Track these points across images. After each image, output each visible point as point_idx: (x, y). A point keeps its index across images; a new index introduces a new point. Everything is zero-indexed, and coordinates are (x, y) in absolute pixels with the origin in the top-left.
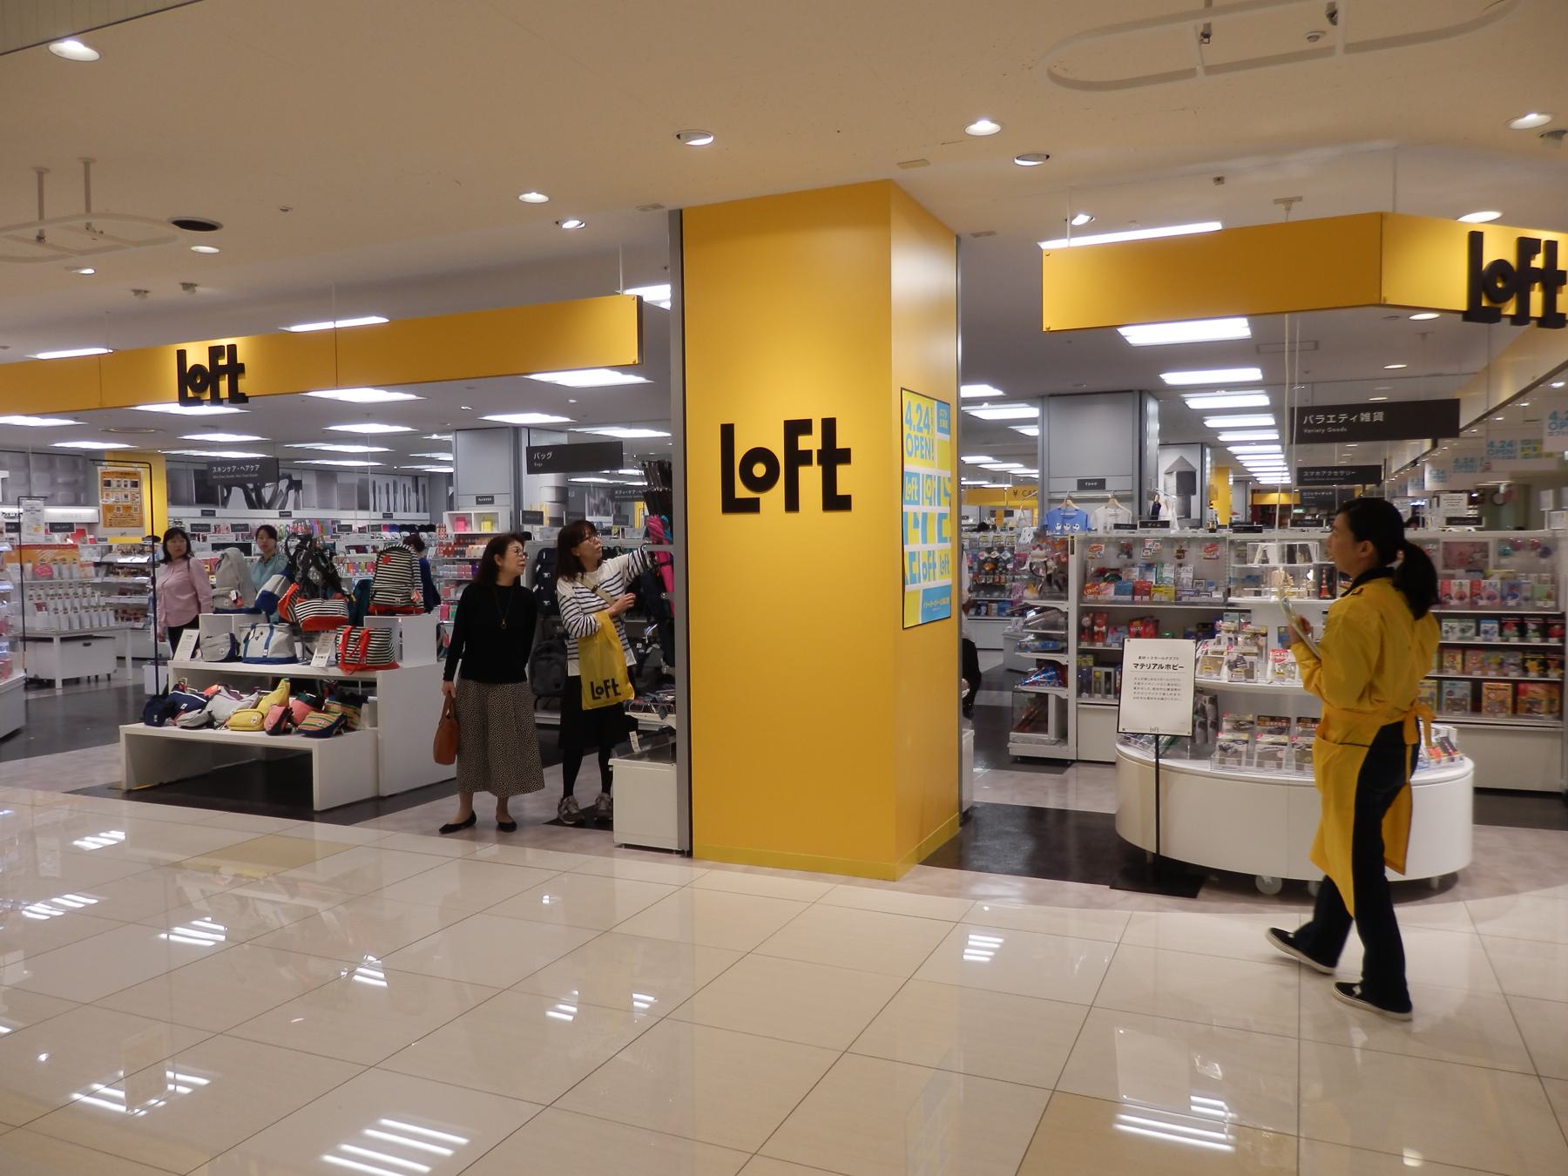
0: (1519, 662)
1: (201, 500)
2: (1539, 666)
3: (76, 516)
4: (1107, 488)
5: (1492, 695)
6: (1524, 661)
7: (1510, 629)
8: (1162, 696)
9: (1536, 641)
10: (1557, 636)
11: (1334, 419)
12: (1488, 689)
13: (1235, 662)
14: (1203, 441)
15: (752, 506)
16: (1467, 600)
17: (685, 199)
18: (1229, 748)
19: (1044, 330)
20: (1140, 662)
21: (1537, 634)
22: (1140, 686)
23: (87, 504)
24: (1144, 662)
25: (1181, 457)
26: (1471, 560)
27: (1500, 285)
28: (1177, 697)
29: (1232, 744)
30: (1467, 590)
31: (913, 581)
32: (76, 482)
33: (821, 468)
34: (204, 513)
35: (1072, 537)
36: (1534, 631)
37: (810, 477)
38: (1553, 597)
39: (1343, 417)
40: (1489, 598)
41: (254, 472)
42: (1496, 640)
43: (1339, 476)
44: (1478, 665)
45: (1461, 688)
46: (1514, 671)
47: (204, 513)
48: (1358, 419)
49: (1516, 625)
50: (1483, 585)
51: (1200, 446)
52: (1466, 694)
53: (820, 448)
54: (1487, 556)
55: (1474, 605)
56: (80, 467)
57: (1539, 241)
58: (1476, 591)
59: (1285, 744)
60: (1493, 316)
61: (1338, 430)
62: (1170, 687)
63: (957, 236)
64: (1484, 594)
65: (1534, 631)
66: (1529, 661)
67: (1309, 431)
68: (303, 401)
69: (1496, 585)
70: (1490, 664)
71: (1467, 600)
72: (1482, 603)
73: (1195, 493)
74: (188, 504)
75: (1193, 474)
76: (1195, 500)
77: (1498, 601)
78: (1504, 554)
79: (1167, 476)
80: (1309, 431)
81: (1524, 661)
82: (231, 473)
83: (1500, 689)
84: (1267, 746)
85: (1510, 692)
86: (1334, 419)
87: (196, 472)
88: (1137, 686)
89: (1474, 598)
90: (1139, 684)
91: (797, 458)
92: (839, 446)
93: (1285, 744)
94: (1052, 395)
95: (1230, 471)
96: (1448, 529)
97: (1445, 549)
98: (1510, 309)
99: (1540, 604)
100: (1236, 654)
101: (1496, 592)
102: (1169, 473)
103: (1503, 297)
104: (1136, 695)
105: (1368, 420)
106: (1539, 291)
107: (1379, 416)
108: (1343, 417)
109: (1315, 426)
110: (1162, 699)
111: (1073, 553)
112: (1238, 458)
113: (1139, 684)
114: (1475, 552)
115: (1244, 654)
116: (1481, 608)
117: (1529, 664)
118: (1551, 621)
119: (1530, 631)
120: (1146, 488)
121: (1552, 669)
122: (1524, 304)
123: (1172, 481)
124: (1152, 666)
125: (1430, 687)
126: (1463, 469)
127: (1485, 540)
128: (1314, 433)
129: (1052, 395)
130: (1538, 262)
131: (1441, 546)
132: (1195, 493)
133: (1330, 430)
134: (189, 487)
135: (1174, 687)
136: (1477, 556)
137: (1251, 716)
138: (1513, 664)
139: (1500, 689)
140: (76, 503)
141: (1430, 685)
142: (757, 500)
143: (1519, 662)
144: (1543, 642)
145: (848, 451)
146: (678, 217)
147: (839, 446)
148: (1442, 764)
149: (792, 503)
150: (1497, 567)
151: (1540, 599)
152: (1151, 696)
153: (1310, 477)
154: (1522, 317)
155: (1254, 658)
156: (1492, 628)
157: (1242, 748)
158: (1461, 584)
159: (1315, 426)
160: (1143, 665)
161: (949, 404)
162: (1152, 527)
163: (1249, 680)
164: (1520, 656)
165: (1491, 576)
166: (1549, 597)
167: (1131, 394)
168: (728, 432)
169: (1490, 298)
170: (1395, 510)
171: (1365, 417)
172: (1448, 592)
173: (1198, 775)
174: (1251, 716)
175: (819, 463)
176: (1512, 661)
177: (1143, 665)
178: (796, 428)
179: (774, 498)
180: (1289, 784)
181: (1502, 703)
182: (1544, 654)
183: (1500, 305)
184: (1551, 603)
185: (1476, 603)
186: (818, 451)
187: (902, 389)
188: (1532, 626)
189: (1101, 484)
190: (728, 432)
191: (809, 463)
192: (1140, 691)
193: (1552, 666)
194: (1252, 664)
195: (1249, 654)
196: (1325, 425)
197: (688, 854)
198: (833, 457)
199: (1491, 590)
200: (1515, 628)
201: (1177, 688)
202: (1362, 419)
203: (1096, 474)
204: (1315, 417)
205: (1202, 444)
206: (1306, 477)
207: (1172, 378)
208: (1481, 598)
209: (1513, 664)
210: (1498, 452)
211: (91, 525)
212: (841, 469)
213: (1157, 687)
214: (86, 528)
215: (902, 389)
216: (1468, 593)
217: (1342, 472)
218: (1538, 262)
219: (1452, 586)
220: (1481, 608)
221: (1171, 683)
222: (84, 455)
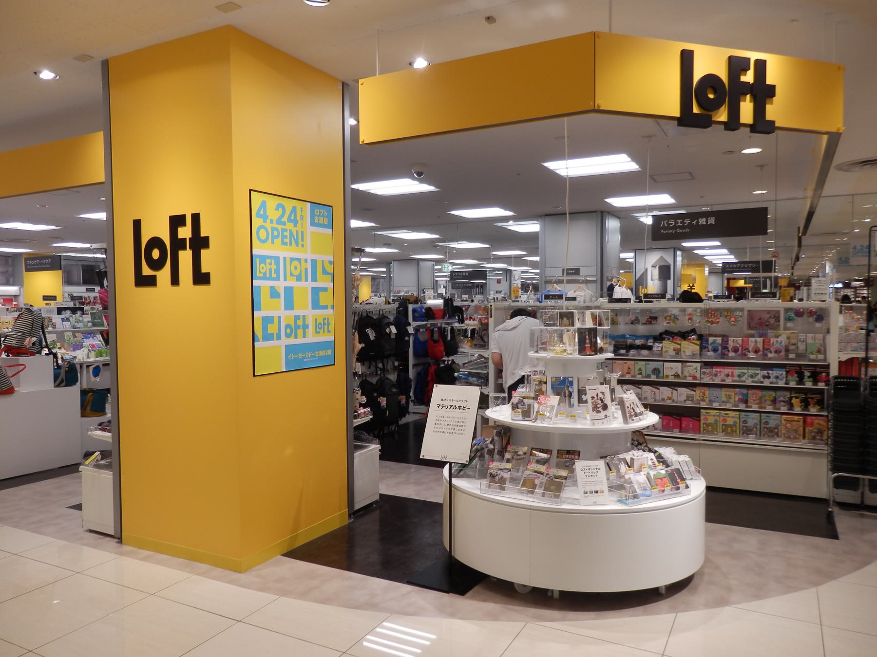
0: (787, 399)
1: (85, 282)
2: (801, 403)
3: (6, 291)
4: (581, 274)
5: (789, 425)
6: (791, 398)
7: (792, 376)
8: (453, 431)
9: (809, 385)
10: (825, 382)
11: (681, 223)
12: (785, 420)
13: (517, 404)
14: (675, 247)
15: (151, 282)
16: (761, 353)
17: (109, 53)
18: (497, 475)
19: (360, 143)
20: (441, 403)
21: (811, 379)
22: (439, 422)
23: (13, 284)
24: (445, 403)
25: (661, 256)
26: (767, 323)
27: (711, 96)
28: (462, 432)
29: (499, 472)
30: (760, 346)
31: (268, 337)
32: (7, 271)
33: (191, 251)
34: (88, 290)
35: (491, 306)
36: (809, 377)
37: (185, 257)
38: (822, 352)
39: (687, 221)
40: (776, 352)
41: (48, 264)
42: (781, 384)
43: (748, 267)
44: (757, 401)
45: (753, 418)
46: (784, 406)
47: (88, 290)
48: (697, 222)
49: (797, 372)
50: (771, 342)
51: (673, 249)
52: (756, 423)
53: (191, 237)
54: (779, 321)
55: (744, 355)
56: (10, 262)
57: (749, 59)
58: (766, 347)
59: (542, 474)
60: (704, 122)
61: (684, 231)
62: (459, 424)
63: (343, 84)
64: (772, 349)
65: (809, 377)
66: (794, 398)
67: (665, 232)
68: (84, 221)
69: (781, 342)
70: (765, 401)
71: (761, 353)
72: (770, 355)
73: (670, 279)
74: (78, 284)
75: (668, 267)
76: (670, 283)
77: (783, 353)
78: (789, 319)
79: (653, 268)
80: (665, 232)
81: (791, 398)
82: (36, 265)
83: (794, 421)
84: (531, 473)
85: (801, 423)
86: (681, 223)
87: (83, 266)
88: (437, 422)
89: (766, 352)
90: (438, 420)
91: (178, 244)
92: (202, 235)
93: (542, 474)
94: (546, 215)
95: (706, 266)
96: (106, 288)
97: (749, 315)
98: (722, 116)
99: (812, 357)
100: (518, 398)
101: (781, 348)
102: (654, 266)
103: (715, 105)
104: (436, 430)
105: (704, 223)
106: (751, 102)
107: (712, 221)
108: (687, 221)
109: (669, 228)
110: (452, 433)
111: (491, 317)
112: (706, 257)
113: (438, 420)
114: (770, 318)
115: (524, 398)
116: (770, 359)
117: (794, 401)
118: (818, 370)
119: (806, 377)
120: (606, 274)
121: (812, 405)
122: (734, 113)
123: (656, 272)
124: (449, 407)
125: (733, 417)
126: (845, 264)
127: (777, 309)
128: (667, 233)
129: (546, 215)
130: (749, 77)
131: (746, 313)
132: (670, 279)
133: (678, 231)
134: (78, 275)
135: (461, 424)
136: (772, 321)
137: (526, 448)
138: (783, 401)
139: (794, 421)
140: (7, 283)
141: (734, 416)
142: (155, 276)
143: (787, 399)
144: (814, 385)
145: (207, 239)
146: (105, 64)
147: (202, 235)
148: (666, 493)
149: (175, 280)
150: (786, 329)
151: (812, 353)
152: (445, 430)
153: (730, 268)
154: (733, 123)
155: (532, 401)
156: (781, 374)
157: (507, 475)
158: (756, 342)
159: (669, 228)
160: (443, 406)
161: (332, 207)
162: (552, 299)
163: (527, 419)
164: (788, 394)
165: (780, 335)
166: (819, 351)
167: (595, 214)
168: (137, 224)
169: (700, 105)
170: (609, 286)
171: (702, 221)
172: (747, 347)
173: (466, 493)
174: (526, 448)
175: (190, 248)
176: (782, 399)
177: (443, 406)
178: (177, 221)
179: (164, 275)
180: (531, 508)
181: (796, 431)
182: (805, 394)
183: (712, 113)
184: (821, 357)
185: (767, 355)
186: (190, 238)
187: (250, 190)
188: (807, 374)
189: (577, 271)
190: (137, 224)
191: (184, 248)
192: (438, 426)
193: (811, 403)
194: (529, 405)
195: (528, 398)
196: (675, 227)
197: (119, 538)
198: (199, 243)
199: (778, 345)
200: (796, 375)
201: (464, 424)
202: (700, 223)
203: (573, 265)
204: (668, 221)
205: (674, 248)
206: (727, 268)
207: (618, 202)
208: (771, 352)
209: (783, 401)
210: (859, 252)
211: (16, 296)
212: (204, 252)
213: (449, 423)
214: (13, 298)
215: (250, 190)
216: (761, 349)
217: (750, 265)
218: (749, 77)
219: (750, 343)
220: (770, 359)
221: (460, 420)
222: (12, 256)
